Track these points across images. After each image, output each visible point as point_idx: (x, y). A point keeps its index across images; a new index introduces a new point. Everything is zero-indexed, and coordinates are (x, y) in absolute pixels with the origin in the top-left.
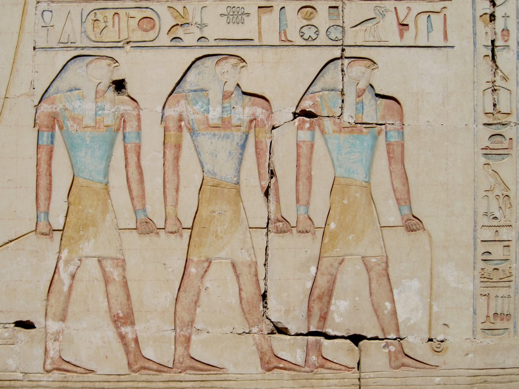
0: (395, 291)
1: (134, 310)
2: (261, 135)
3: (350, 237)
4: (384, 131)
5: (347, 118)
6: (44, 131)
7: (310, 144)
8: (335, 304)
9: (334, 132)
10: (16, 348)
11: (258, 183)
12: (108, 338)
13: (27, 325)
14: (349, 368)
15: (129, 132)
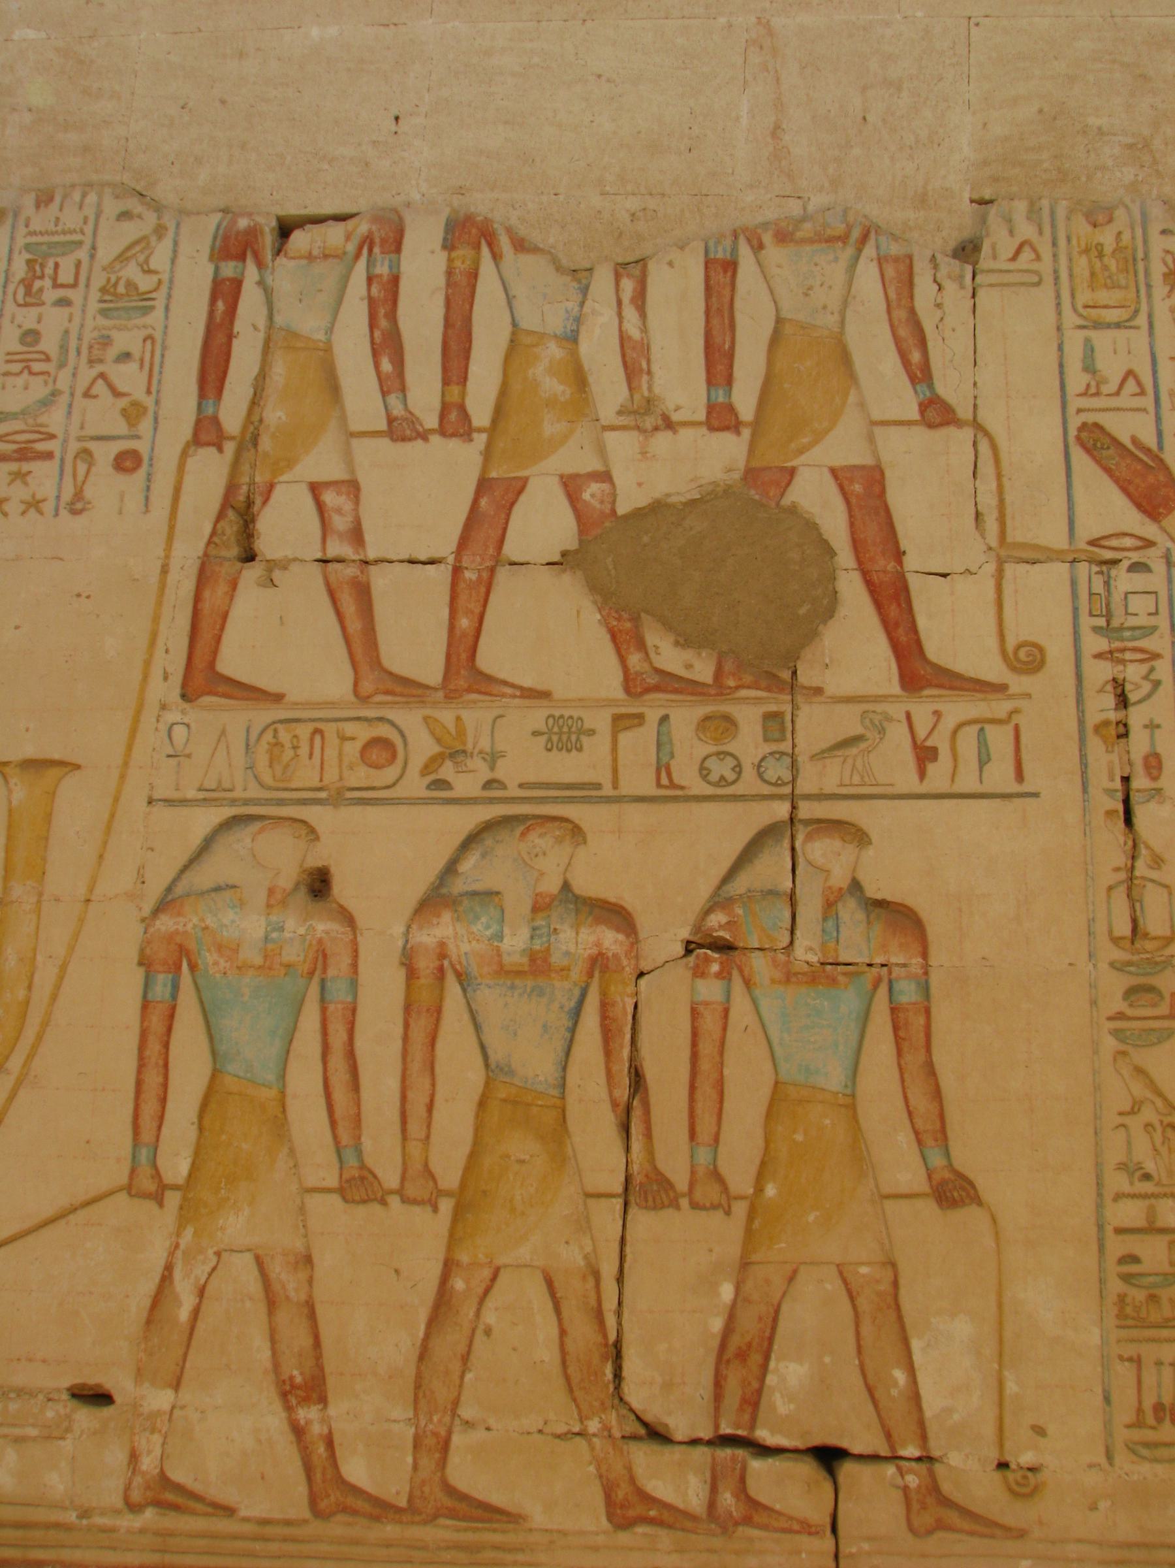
0: (916, 1345)
1: (327, 1370)
2: (613, 988)
3: (811, 1218)
4: (886, 981)
5: (806, 951)
6: (159, 972)
7: (720, 1008)
9: (773, 981)
10: (67, 1445)
11: (604, 1095)
13: (100, 1398)
14: (807, 1528)
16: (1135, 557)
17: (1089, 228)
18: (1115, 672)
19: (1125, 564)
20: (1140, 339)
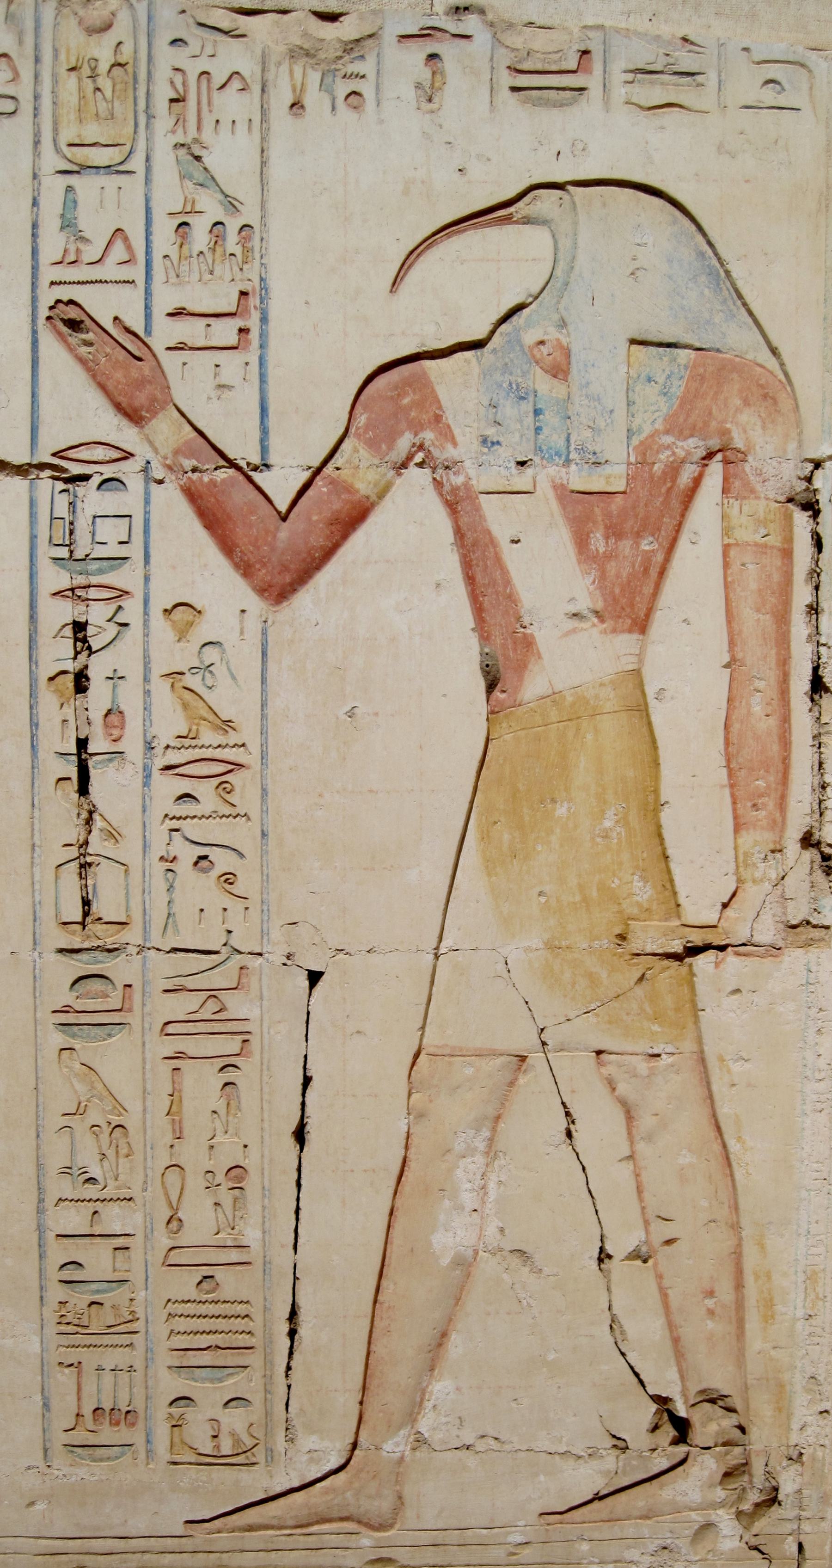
16: (108, 471)
17: (82, 37)
18: (76, 614)
19: (96, 480)
20: (134, 186)
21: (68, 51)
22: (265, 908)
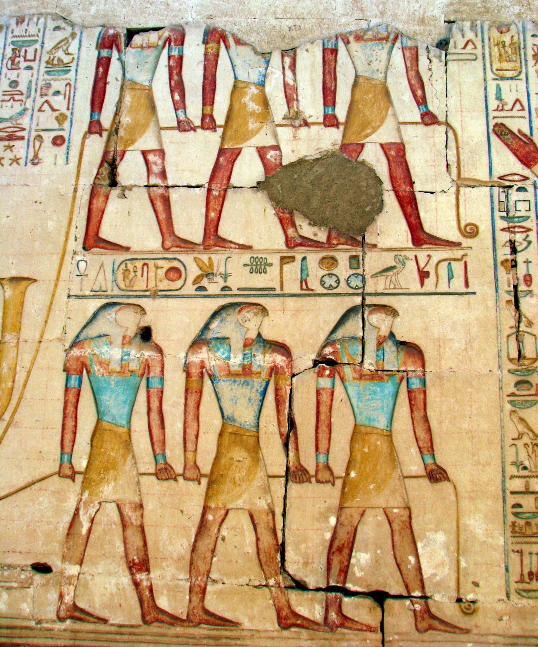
0: (419, 545)
1: (150, 556)
2: (281, 382)
4: (405, 378)
5: (369, 365)
7: (330, 391)
8: (356, 556)
9: (354, 378)
12: (123, 584)
14: (370, 629)
15: (154, 377)
16: (520, 184)
19: (515, 188)
20: (522, 85)
21: (494, 39)
22: (499, 345)
